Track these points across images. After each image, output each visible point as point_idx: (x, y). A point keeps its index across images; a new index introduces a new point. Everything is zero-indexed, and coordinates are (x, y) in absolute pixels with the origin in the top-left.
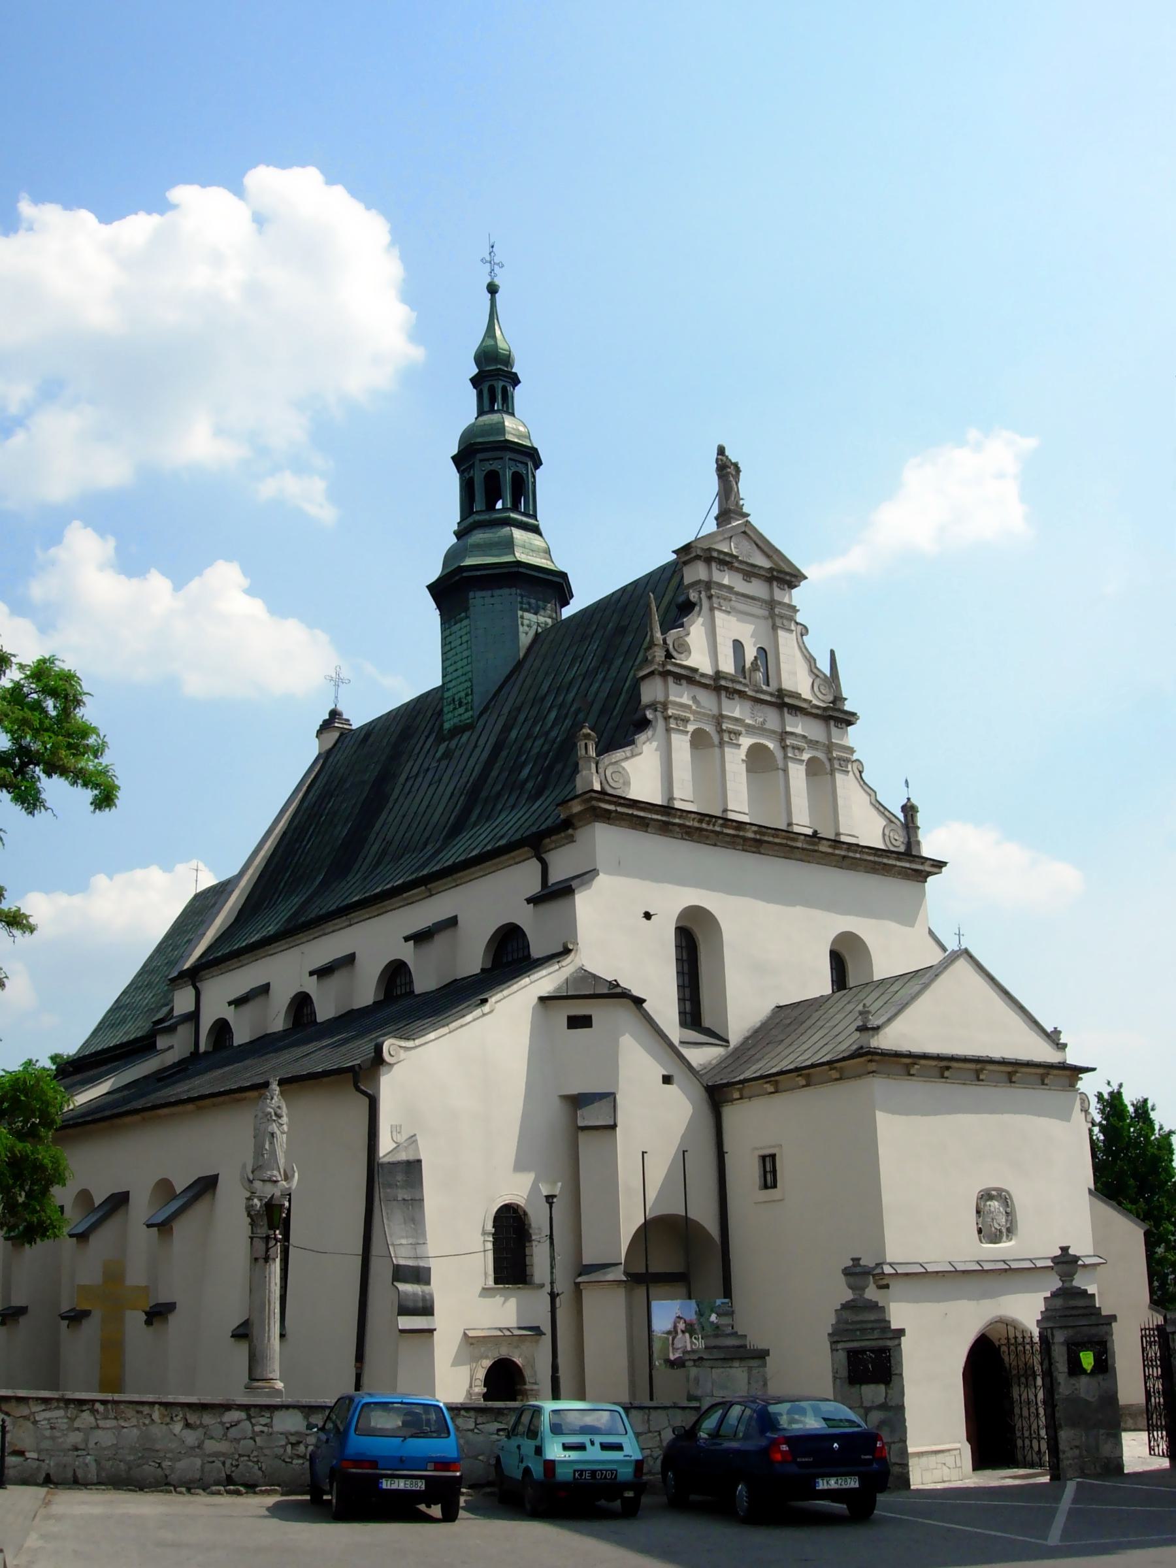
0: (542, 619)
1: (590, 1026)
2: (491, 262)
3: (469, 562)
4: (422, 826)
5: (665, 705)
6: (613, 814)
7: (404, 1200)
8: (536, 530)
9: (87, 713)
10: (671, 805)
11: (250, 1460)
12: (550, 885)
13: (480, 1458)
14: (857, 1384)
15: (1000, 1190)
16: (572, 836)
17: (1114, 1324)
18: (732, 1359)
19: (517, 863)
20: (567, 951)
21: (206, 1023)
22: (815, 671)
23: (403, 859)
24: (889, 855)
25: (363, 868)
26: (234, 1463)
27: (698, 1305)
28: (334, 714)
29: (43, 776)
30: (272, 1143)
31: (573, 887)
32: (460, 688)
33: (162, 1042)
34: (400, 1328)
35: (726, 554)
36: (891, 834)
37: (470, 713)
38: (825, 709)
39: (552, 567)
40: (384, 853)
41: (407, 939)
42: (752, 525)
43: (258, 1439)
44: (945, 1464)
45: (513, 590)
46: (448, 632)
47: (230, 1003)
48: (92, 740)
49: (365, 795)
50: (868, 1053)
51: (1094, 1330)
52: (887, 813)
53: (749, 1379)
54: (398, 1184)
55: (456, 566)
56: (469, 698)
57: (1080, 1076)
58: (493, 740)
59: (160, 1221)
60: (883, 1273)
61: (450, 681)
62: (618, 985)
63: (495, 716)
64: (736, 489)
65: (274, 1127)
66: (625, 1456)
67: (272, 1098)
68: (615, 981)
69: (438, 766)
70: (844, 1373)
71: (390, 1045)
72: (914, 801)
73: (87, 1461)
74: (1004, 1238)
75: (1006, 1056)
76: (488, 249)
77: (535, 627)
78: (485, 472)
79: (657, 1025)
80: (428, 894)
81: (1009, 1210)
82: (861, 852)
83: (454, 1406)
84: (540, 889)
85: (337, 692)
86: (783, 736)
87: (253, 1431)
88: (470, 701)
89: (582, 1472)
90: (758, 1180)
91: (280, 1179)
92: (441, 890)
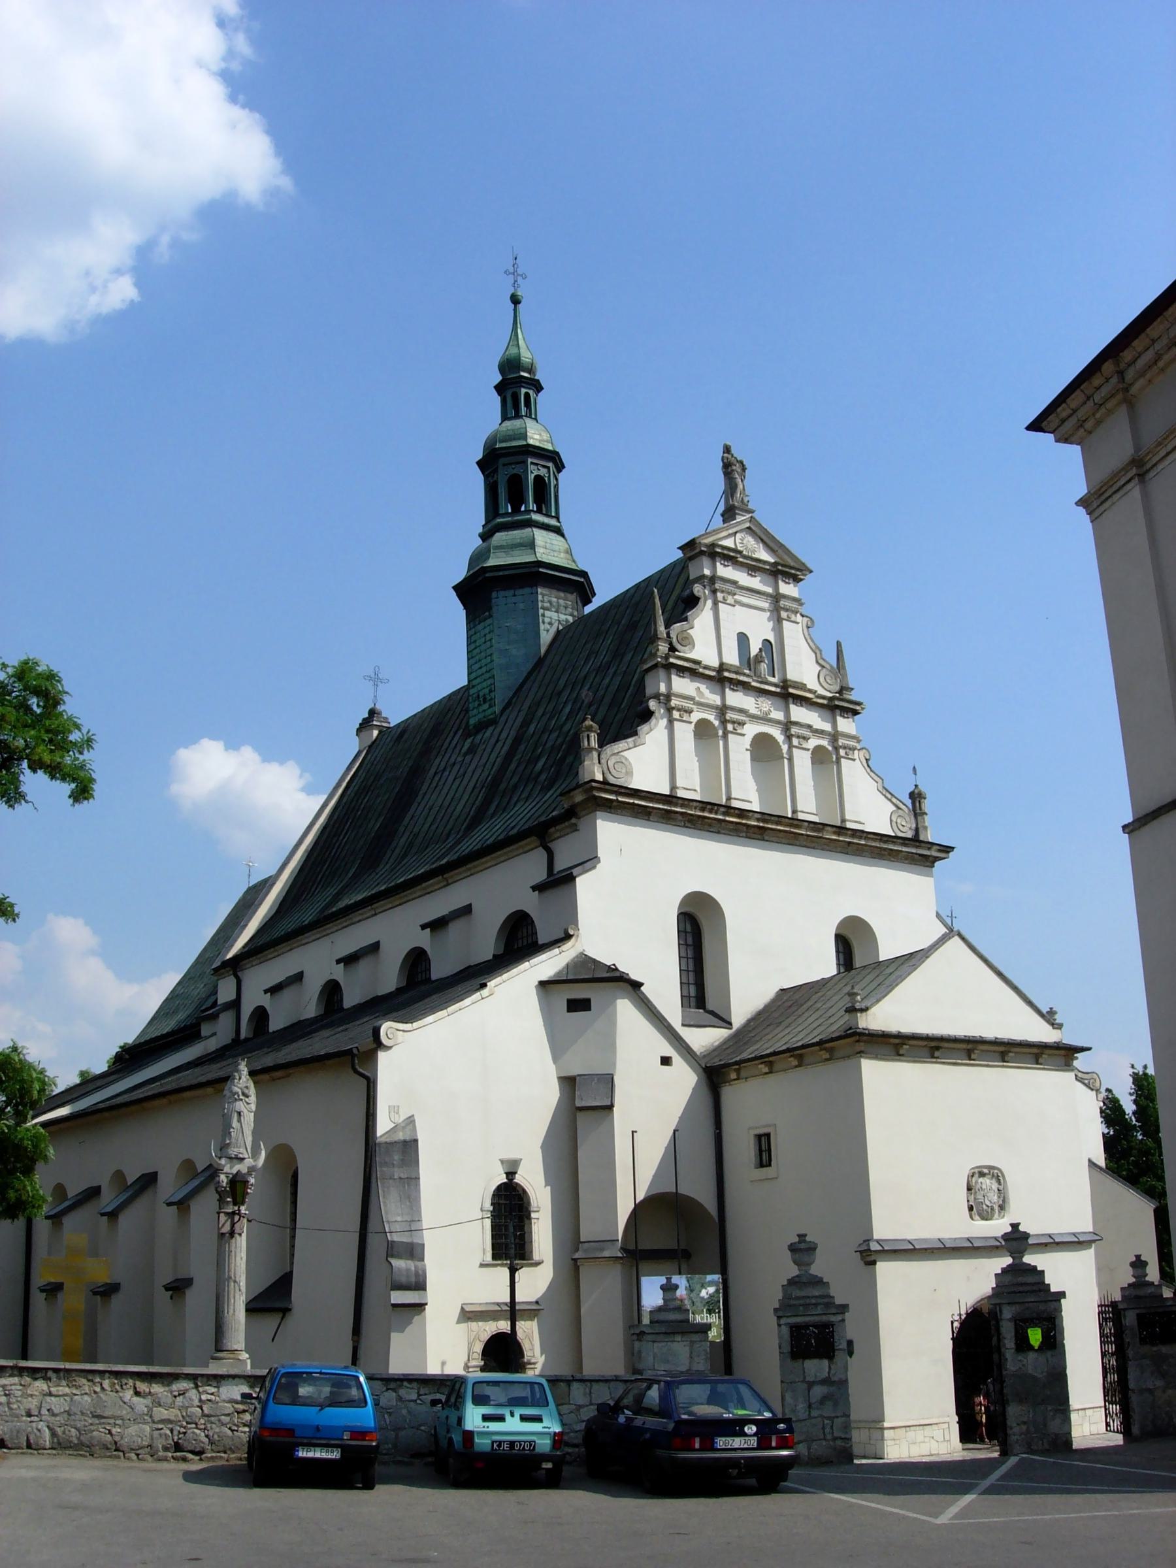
0: (563, 617)
1: (589, 1009)
2: (515, 273)
3: (492, 562)
5: (668, 697)
6: (615, 804)
7: (400, 1178)
8: (558, 531)
9: (70, 707)
10: (674, 794)
11: (197, 1428)
12: (555, 872)
13: (423, 1428)
14: (799, 1358)
15: (991, 1168)
16: (575, 825)
17: (1063, 1301)
18: (673, 1333)
20: (568, 937)
21: (247, 1010)
22: (821, 662)
23: (427, 851)
24: (895, 840)
25: (392, 860)
26: (183, 1430)
27: (688, 1281)
28: (373, 713)
29: (27, 772)
30: (239, 1121)
31: (574, 874)
32: (484, 685)
33: (205, 1030)
34: (392, 1302)
35: (729, 549)
36: (899, 821)
38: (831, 699)
39: (574, 567)
40: (411, 845)
41: (423, 927)
42: (756, 521)
43: (205, 1408)
44: (933, 1437)
46: (473, 631)
47: (266, 992)
48: (75, 736)
49: (397, 790)
50: (855, 1034)
51: (1042, 1307)
52: (894, 800)
53: (691, 1353)
54: (395, 1162)
55: (480, 566)
56: (492, 694)
57: (1076, 1055)
58: (513, 733)
59: (176, 1200)
60: (869, 1250)
61: (475, 678)
62: (616, 969)
63: (515, 713)
64: (741, 486)
65: (240, 1106)
66: (545, 1427)
67: (240, 1078)
68: (614, 965)
70: (787, 1348)
71: (388, 1028)
72: (922, 788)
73: (40, 1427)
74: (996, 1216)
75: (999, 1036)
76: (511, 261)
79: (656, 1008)
80: (445, 883)
81: (1001, 1188)
82: (866, 838)
83: (396, 1377)
84: (546, 877)
86: (787, 726)
87: (200, 1400)
89: (500, 1443)
90: (754, 1159)
91: (246, 1156)
92: (456, 879)
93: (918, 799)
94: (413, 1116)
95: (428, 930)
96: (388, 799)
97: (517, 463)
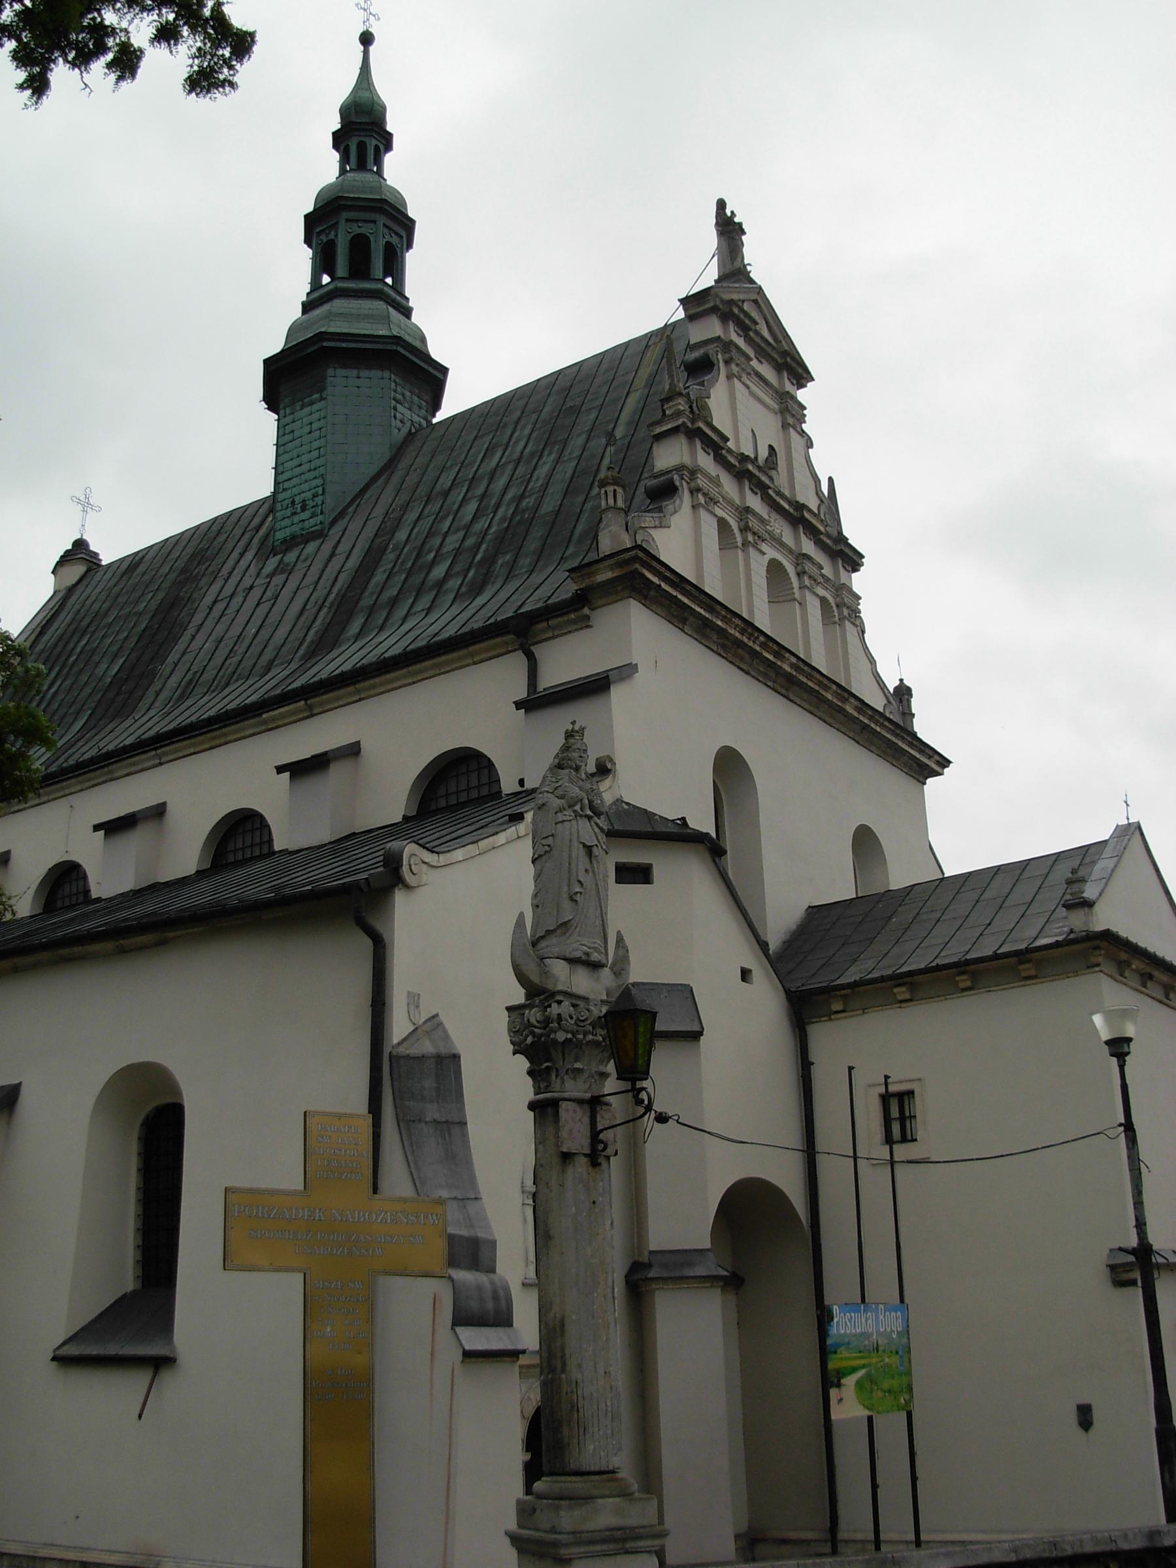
0: (416, 419)
4: (255, 649)
6: (652, 593)
16: (588, 618)
19: (475, 663)
32: (305, 487)
37: (320, 518)
41: (280, 769)
45: (386, 374)
56: (319, 500)
69: (269, 583)
77: (408, 424)
78: (352, 235)
85: (84, 519)
88: (319, 503)
93: (906, 697)
94: (437, 1015)
95: (287, 775)
96: (126, 638)
97: (365, 221)
